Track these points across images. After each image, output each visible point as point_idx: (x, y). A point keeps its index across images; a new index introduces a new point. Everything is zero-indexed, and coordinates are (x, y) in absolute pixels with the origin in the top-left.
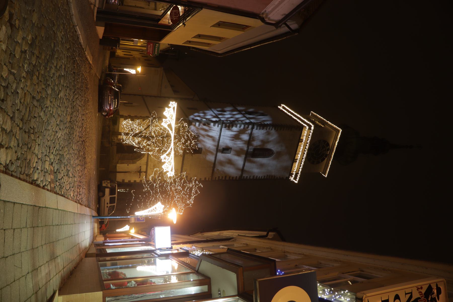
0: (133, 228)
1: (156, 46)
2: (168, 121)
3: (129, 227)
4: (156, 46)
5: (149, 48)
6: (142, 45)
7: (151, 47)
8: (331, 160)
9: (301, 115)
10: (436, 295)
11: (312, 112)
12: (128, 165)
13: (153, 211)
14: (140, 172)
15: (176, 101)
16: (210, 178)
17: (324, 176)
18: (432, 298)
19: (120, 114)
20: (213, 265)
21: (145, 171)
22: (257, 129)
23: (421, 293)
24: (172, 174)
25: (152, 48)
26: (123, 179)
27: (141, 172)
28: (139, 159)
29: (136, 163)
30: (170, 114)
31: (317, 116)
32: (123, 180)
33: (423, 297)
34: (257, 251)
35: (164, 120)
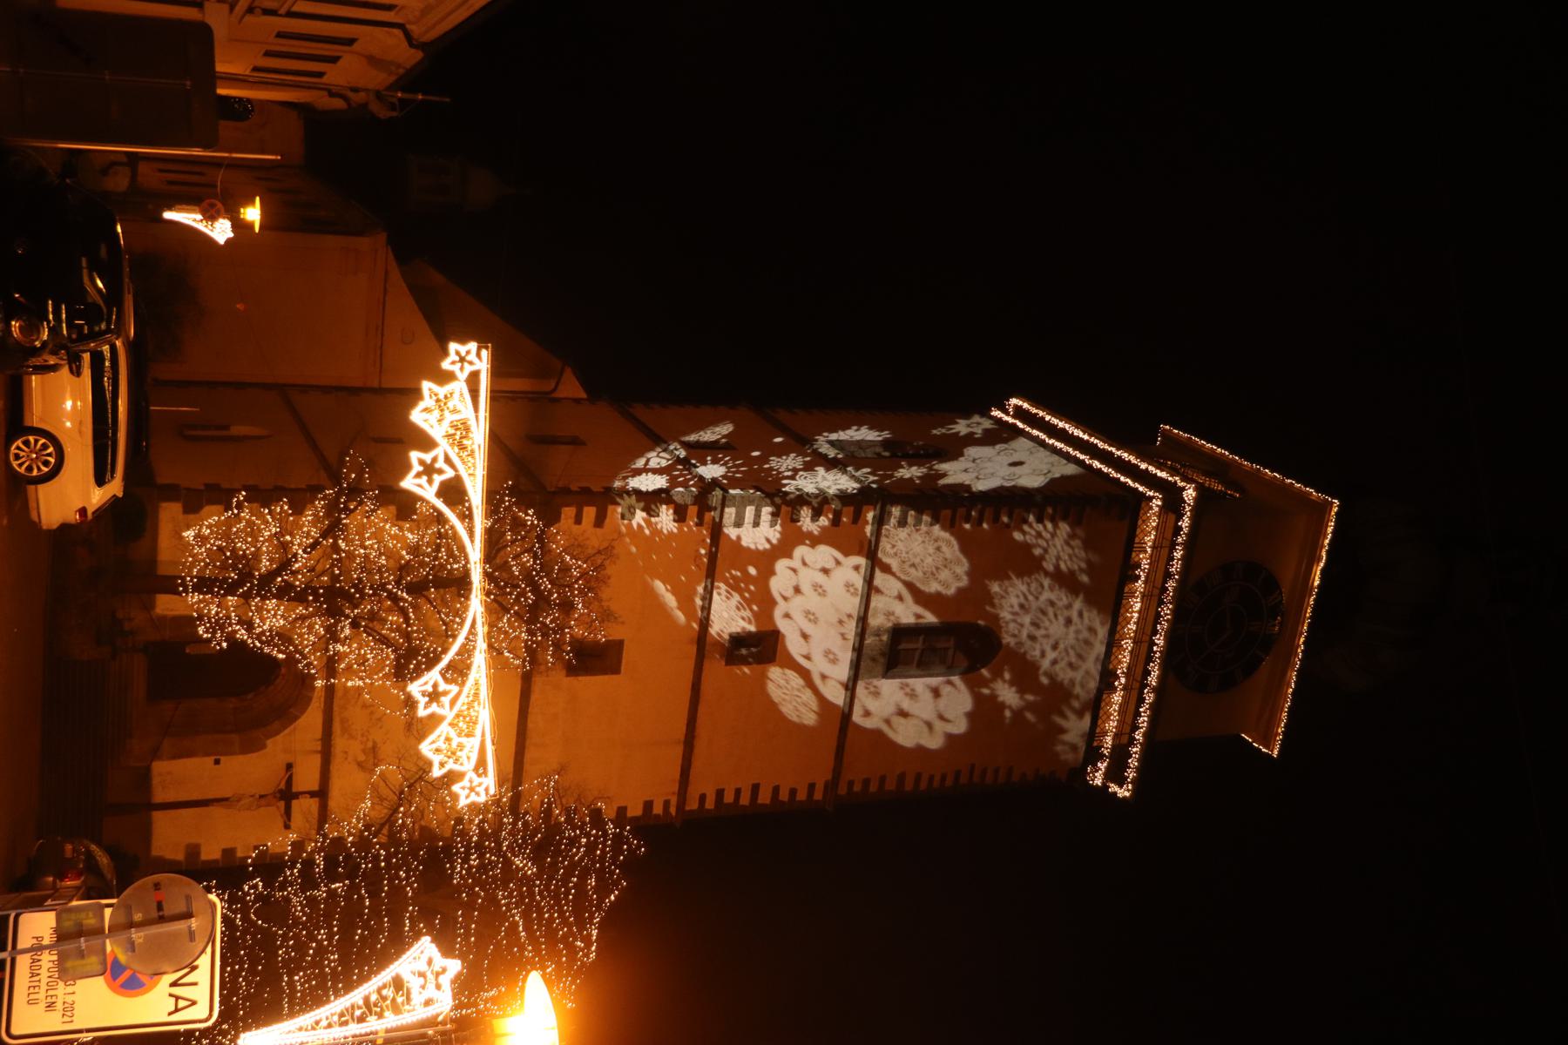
2: (440, 464)
6: (255, 69)
14: (287, 795)
15: (482, 341)
16: (674, 801)
19: (160, 481)
21: (316, 787)
22: (902, 523)
24: (481, 790)
26: (193, 841)
27: (297, 796)
29: (264, 746)
30: (449, 417)
35: (414, 456)
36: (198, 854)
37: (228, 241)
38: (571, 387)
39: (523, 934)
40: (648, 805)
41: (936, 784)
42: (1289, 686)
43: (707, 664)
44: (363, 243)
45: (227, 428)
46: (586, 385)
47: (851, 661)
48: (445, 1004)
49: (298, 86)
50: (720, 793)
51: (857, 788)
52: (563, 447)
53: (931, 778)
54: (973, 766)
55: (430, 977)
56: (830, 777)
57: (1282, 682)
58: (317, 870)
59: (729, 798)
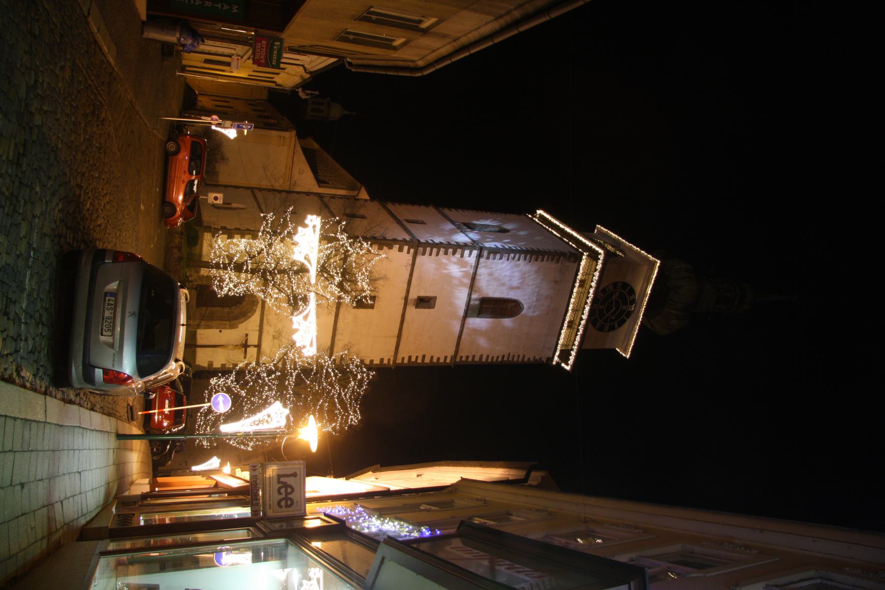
0: (228, 463)
1: (275, 45)
3: (219, 461)
4: (275, 47)
5: (258, 50)
6: (249, 75)
7: (263, 48)
8: (639, 324)
9: (574, 229)
11: (599, 226)
12: (220, 331)
13: (263, 424)
14: (245, 346)
16: (392, 359)
17: (624, 355)
20: (421, 579)
21: (256, 344)
25: (264, 49)
26: (211, 360)
27: (249, 346)
28: (243, 319)
29: (238, 327)
31: (609, 233)
32: (211, 364)
34: (511, 517)
36: (212, 365)
37: (235, 138)
38: (364, 195)
39: (318, 407)
40: (382, 360)
41: (495, 359)
42: (635, 331)
43: (408, 307)
44: (287, 134)
45: (230, 204)
46: (369, 194)
47: (465, 310)
48: (283, 423)
50: (410, 357)
51: (464, 359)
52: (359, 219)
53: (493, 357)
54: (510, 354)
55: (279, 414)
56: (453, 354)
57: (633, 329)
59: (413, 359)
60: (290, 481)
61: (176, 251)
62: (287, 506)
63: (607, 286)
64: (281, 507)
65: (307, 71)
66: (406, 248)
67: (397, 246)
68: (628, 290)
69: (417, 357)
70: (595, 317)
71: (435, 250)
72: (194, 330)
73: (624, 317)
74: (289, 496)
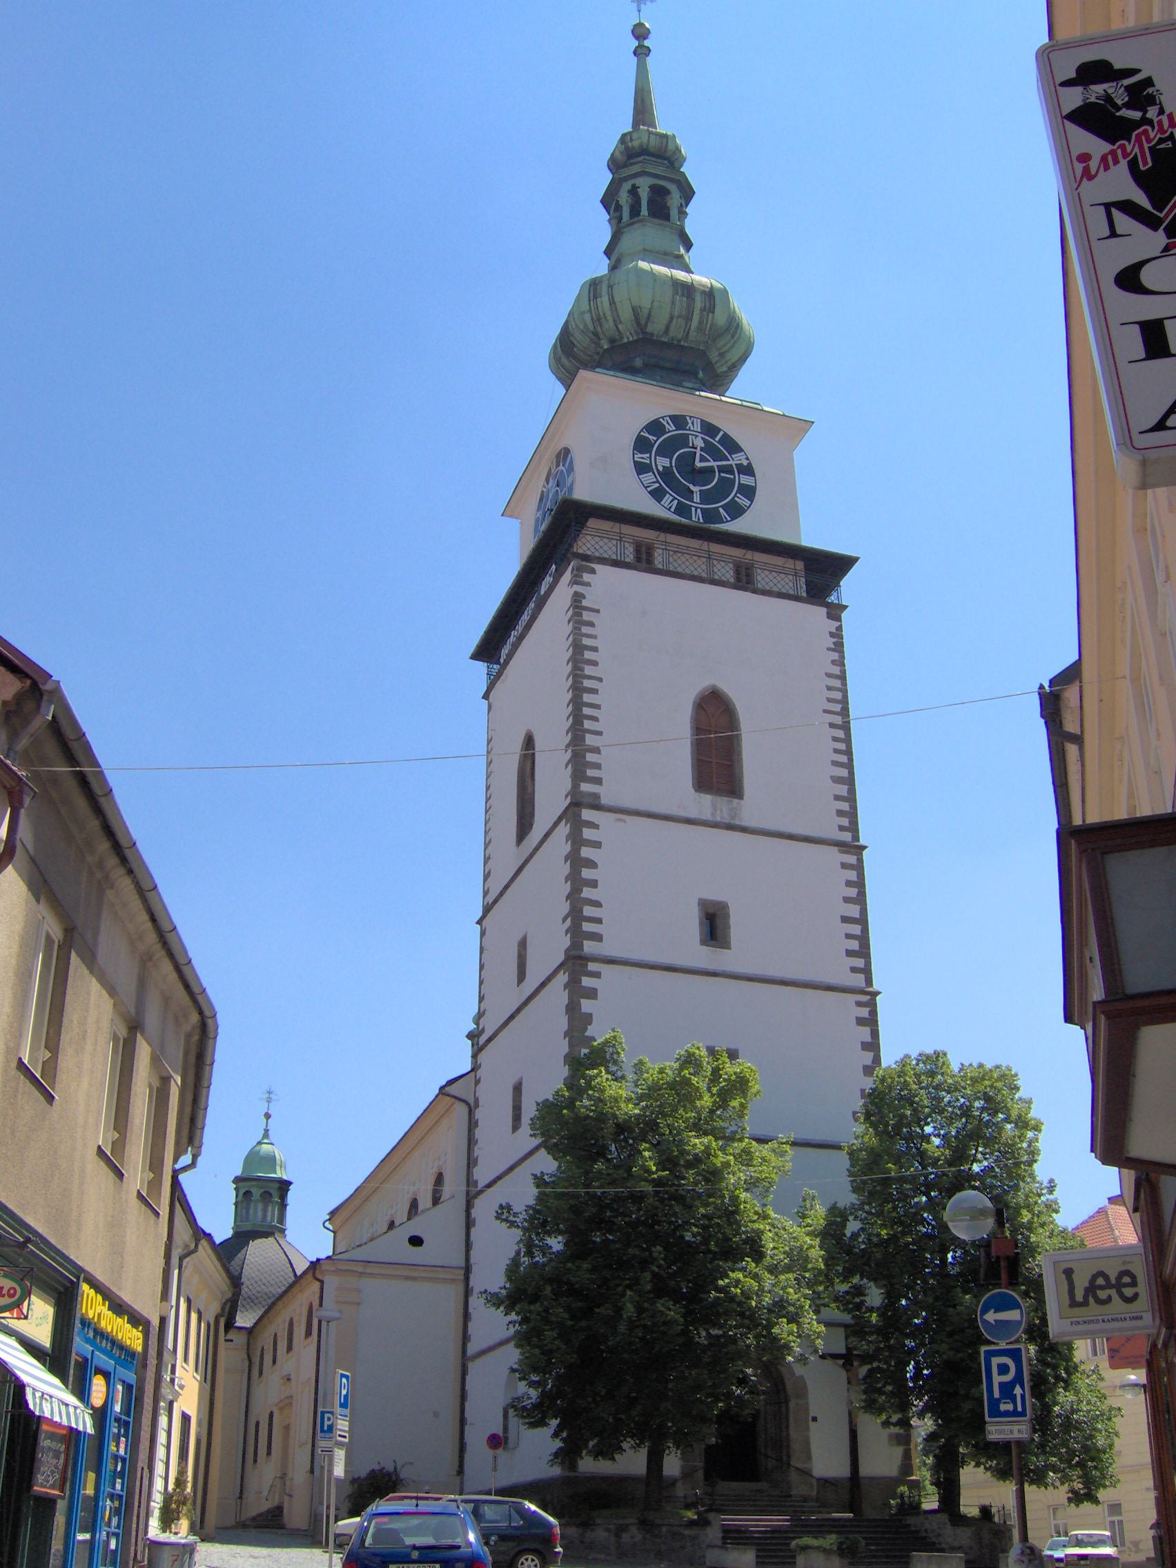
10: (1115, 84)
18: (1128, 106)
23: (1110, 158)
29: (802, 1377)
33: (1129, 148)
49: (193, 1120)
58: (921, 1404)
60: (1081, 1283)
61: (626, 1537)
62: (1134, 1284)
63: (646, 488)
64: (1136, 1296)
65: (193, 1246)
66: (586, 982)
67: (583, 1001)
68: (647, 435)
69: (848, 936)
70: (721, 509)
71: (588, 911)
72: (815, 1483)
73: (717, 439)
74: (1113, 1282)
